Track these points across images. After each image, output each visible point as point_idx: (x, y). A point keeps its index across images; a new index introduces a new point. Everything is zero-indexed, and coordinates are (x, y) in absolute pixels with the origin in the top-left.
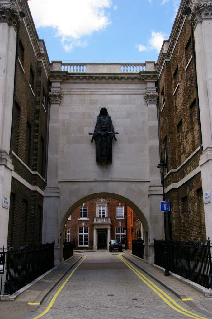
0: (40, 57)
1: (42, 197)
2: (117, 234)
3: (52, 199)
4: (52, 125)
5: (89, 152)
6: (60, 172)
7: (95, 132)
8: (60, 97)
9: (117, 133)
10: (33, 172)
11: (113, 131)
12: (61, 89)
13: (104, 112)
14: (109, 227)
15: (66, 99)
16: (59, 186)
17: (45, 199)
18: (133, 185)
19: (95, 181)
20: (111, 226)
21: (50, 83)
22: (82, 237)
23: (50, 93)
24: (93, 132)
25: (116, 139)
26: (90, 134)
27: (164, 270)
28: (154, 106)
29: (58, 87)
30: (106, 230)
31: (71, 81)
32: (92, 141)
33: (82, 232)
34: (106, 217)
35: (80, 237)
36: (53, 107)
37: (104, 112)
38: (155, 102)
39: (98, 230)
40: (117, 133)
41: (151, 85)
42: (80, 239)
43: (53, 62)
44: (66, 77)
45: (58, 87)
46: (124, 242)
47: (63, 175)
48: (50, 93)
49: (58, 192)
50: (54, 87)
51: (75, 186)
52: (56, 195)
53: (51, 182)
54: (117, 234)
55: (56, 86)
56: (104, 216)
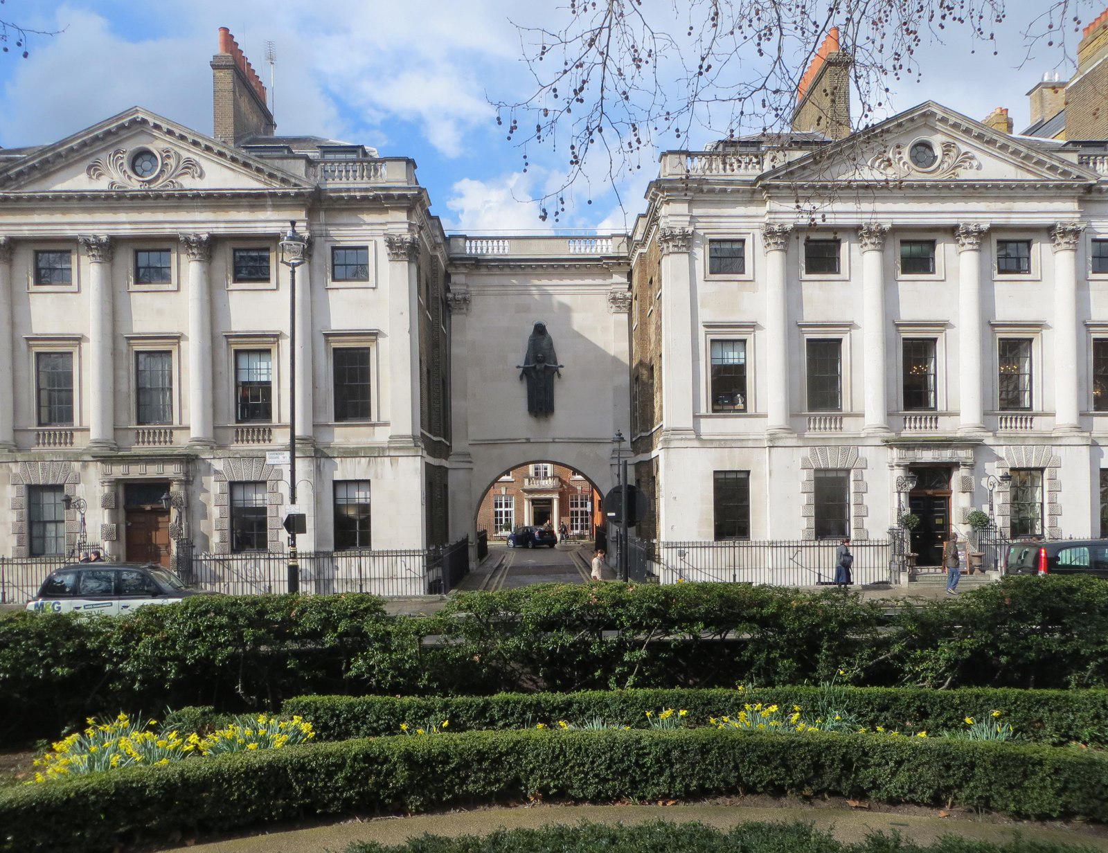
0: (435, 248)
1: (446, 469)
2: (571, 509)
3: (461, 472)
4: (455, 351)
5: (518, 394)
6: (471, 429)
7: (526, 363)
8: (466, 300)
9: (562, 366)
10: (435, 439)
11: (556, 362)
12: (468, 286)
13: (540, 330)
14: (555, 497)
15: (477, 304)
16: (471, 450)
17: (450, 472)
18: (587, 449)
19: (528, 441)
20: (561, 494)
21: (448, 276)
22: (501, 515)
23: (450, 296)
24: (522, 365)
25: (559, 375)
26: (518, 367)
27: (154, 533)
28: (625, 317)
29: (462, 285)
30: (550, 501)
31: (484, 271)
32: (521, 378)
33: (577, 506)
34: (549, 475)
35: (496, 515)
36: (455, 318)
37: (540, 330)
38: (626, 310)
39: (534, 501)
40: (562, 366)
41: (619, 279)
42: (496, 520)
43: (452, 237)
44: (478, 264)
45: (462, 285)
46: (587, 526)
47: (475, 433)
48: (450, 296)
49: (470, 462)
50: (455, 284)
51: (496, 451)
52: (468, 465)
53: (458, 445)
54: (571, 509)
55: (459, 281)
56: (546, 473)
